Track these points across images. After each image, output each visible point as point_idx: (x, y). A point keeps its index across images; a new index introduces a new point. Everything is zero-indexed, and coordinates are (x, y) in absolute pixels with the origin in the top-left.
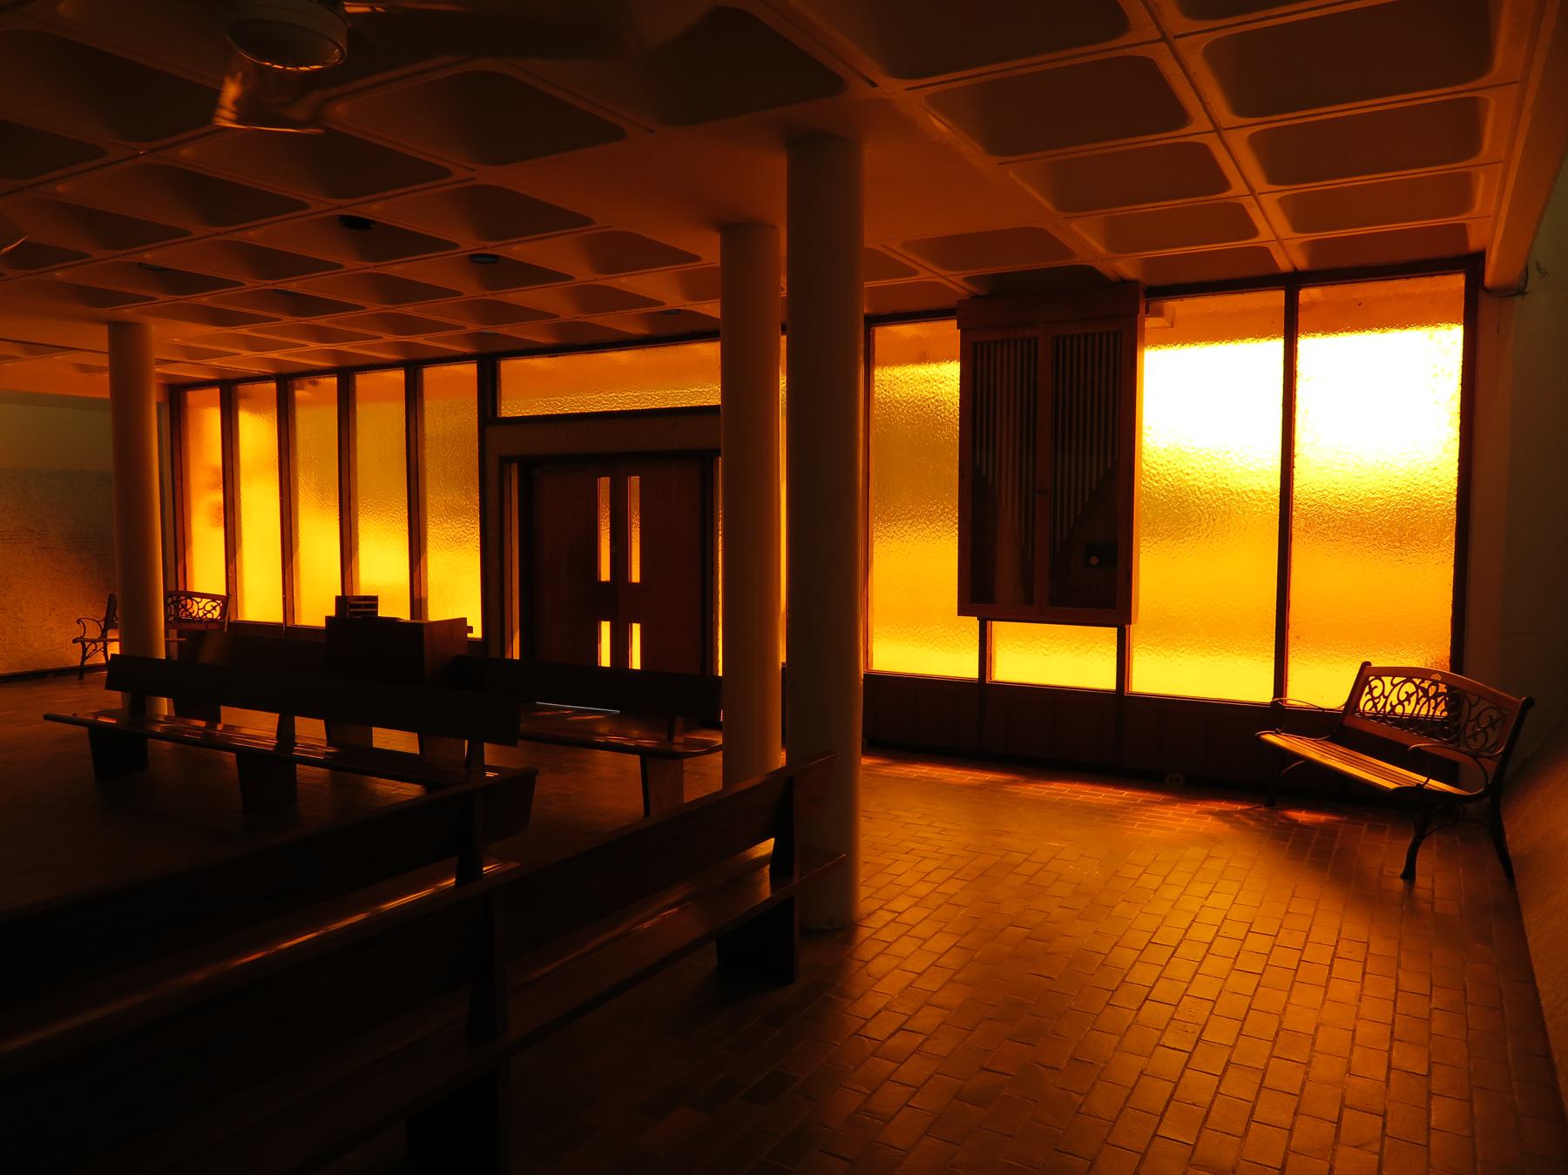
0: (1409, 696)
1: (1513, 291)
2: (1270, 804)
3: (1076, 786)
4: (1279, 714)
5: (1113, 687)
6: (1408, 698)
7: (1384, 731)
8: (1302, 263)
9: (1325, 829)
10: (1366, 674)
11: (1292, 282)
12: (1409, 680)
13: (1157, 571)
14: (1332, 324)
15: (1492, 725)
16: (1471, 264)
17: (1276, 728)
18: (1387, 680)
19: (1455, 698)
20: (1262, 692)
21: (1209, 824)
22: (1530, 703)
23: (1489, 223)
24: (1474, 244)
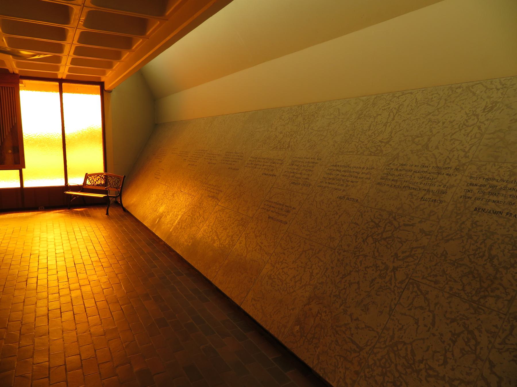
0: (99, 179)
1: (110, 92)
2: (69, 209)
3: (14, 214)
4: (67, 187)
5: (20, 186)
6: (99, 179)
7: (94, 188)
8: (64, 77)
9: (84, 210)
10: (87, 176)
11: (61, 81)
12: (98, 176)
13: (30, 154)
14: (69, 91)
15: (118, 182)
16: (102, 84)
17: (68, 191)
18: (93, 176)
19: (106, 178)
20: (63, 184)
21: (58, 214)
22: (125, 177)
23: (110, 78)
24: (102, 80)
